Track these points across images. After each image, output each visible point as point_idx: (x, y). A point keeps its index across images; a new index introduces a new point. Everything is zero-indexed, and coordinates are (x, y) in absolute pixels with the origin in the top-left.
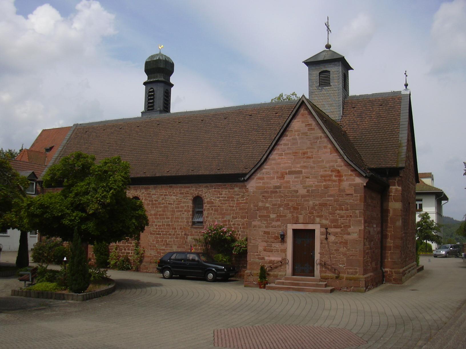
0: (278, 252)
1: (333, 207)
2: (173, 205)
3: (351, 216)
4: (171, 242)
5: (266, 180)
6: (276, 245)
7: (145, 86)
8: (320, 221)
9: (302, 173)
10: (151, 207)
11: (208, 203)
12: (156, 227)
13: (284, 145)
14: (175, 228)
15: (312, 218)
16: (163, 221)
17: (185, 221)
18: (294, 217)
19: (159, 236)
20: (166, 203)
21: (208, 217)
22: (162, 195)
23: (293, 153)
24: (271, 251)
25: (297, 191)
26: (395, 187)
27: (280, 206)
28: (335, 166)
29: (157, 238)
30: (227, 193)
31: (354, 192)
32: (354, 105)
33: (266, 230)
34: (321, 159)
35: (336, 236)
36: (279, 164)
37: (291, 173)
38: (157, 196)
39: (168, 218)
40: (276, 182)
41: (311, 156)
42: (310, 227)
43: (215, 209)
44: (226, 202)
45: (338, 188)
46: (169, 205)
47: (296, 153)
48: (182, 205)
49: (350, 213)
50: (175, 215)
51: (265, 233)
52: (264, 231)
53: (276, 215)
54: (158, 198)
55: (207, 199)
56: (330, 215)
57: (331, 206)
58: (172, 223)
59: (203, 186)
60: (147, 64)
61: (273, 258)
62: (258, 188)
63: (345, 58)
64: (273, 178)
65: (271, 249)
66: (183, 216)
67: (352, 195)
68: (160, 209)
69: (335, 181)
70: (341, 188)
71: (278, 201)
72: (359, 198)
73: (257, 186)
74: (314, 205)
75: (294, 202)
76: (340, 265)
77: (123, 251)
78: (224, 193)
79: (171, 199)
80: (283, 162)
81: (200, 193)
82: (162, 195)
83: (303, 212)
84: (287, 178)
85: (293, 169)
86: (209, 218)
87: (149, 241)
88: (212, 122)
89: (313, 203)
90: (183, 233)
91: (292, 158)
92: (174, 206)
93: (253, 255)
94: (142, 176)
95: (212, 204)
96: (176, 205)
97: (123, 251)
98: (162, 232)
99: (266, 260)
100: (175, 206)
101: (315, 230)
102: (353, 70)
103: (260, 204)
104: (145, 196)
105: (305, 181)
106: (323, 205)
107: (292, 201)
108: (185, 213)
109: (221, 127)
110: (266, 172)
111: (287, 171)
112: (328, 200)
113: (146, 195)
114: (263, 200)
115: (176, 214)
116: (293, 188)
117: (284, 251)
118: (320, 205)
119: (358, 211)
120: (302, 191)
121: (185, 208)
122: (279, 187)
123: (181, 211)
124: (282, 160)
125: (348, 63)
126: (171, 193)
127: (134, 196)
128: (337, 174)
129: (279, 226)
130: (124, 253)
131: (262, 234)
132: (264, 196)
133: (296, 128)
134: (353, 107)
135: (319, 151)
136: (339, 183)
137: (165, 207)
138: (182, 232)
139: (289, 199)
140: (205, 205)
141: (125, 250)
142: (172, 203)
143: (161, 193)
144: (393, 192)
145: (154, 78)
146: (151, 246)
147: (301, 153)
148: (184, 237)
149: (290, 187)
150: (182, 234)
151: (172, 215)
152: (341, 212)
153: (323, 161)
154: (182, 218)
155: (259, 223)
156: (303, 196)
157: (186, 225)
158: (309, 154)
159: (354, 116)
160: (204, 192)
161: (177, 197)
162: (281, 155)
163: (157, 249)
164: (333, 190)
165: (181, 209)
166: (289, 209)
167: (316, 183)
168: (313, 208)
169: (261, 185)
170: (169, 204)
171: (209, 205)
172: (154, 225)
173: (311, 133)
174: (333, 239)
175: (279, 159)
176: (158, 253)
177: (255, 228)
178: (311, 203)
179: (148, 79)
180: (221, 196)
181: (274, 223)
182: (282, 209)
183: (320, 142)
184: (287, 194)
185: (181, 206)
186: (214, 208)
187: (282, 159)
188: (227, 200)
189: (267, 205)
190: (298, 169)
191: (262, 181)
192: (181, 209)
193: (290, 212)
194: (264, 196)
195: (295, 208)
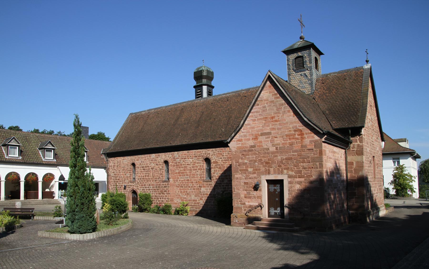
0: (255, 198)
1: (297, 160)
2: (190, 166)
3: (312, 167)
4: (190, 192)
5: (243, 142)
6: (253, 193)
7: (195, 89)
8: (287, 172)
9: (271, 134)
10: (176, 167)
11: (214, 162)
12: (180, 182)
13: (256, 113)
14: (193, 182)
15: (281, 170)
16: (184, 177)
17: (199, 177)
18: (267, 170)
19: (182, 188)
20: (186, 164)
21: (214, 173)
22: (183, 158)
23: (264, 118)
24: (250, 198)
25: (269, 149)
26: (357, 143)
27: (255, 161)
28: (298, 126)
29: (181, 189)
30: (227, 154)
31: (314, 147)
32: (324, 81)
33: (246, 181)
34: (285, 122)
35: (301, 185)
36: (253, 128)
37: (262, 134)
38: (179, 159)
39: (187, 175)
40: (251, 143)
41: (278, 120)
42: (279, 177)
43: (219, 167)
44: (227, 161)
45: (301, 145)
46: (188, 166)
47: (266, 118)
48: (196, 165)
49: (311, 164)
50: (192, 173)
51: (245, 183)
52: (244, 182)
53: (253, 169)
54: (180, 161)
55: (213, 160)
56: (295, 167)
57: (295, 160)
58: (190, 178)
59: (210, 150)
60: (195, 73)
61: (252, 204)
62: (239, 148)
63: (314, 44)
64: (249, 139)
65: (250, 196)
66: (198, 173)
67: (312, 149)
68: (182, 169)
69: (297, 139)
70: (304, 144)
71: (253, 157)
72: (318, 152)
73: (238, 147)
74: (282, 159)
75: (265, 158)
76: (305, 209)
77: (159, 199)
78: (225, 154)
79: (189, 161)
80: (257, 126)
81: (208, 156)
82: (183, 158)
83: (273, 165)
84: (261, 138)
85: (265, 131)
86: (215, 174)
87: (176, 192)
88: (219, 104)
89: (281, 158)
90: (198, 186)
91: (263, 123)
92: (191, 166)
93: (237, 201)
94: (169, 145)
95: (217, 163)
96: (192, 165)
97: (159, 199)
98: (184, 185)
99: (246, 205)
100: (192, 166)
101: (283, 180)
102: (324, 55)
103: (240, 161)
104: (172, 160)
105: (274, 140)
106: (288, 159)
107: (264, 157)
108: (199, 171)
109: (225, 107)
110: (243, 135)
111: (260, 133)
112: (293, 155)
113: (172, 159)
114: (243, 158)
115: (192, 172)
116: (266, 147)
117: (260, 197)
118: (286, 159)
119: (318, 163)
120: (272, 149)
121: (199, 167)
122: (254, 146)
123: (196, 170)
124: (256, 124)
125: (318, 49)
126: (188, 156)
127: (165, 160)
128: (299, 133)
129: (255, 178)
130: (160, 201)
131: (243, 184)
132: (243, 154)
133: (265, 98)
134: (323, 83)
135: (284, 115)
136: (301, 140)
137: (185, 167)
138: (197, 185)
139: (262, 155)
140: (212, 164)
141: (161, 199)
142: (190, 164)
143: (182, 157)
144: (356, 148)
145: (200, 83)
146: (177, 196)
147: (270, 118)
148: (199, 188)
149: (262, 146)
150: (197, 186)
151: (190, 172)
152: (304, 164)
153: (287, 123)
154: (197, 175)
155: (240, 176)
156: (273, 153)
157: (200, 180)
158: (276, 118)
159: (324, 89)
160: (211, 155)
161: (193, 160)
162: (254, 120)
163: (181, 198)
164: (297, 147)
165: (196, 168)
166: (262, 163)
167: (283, 142)
168: (281, 162)
169: (240, 145)
170: (188, 165)
171: (215, 164)
172: (178, 181)
173: (277, 101)
174: (299, 187)
175: (253, 124)
176: (182, 200)
177: (237, 180)
178: (279, 158)
179: (197, 83)
180: (223, 157)
181: (251, 176)
182: (257, 164)
183: (284, 107)
184: (260, 152)
185: (195, 166)
186: (218, 166)
187: (255, 123)
188: (227, 160)
189: (246, 161)
190: (268, 131)
191: (240, 142)
192: (196, 168)
193: (263, 166)
194: (243, 154)
195: (267, 163)
